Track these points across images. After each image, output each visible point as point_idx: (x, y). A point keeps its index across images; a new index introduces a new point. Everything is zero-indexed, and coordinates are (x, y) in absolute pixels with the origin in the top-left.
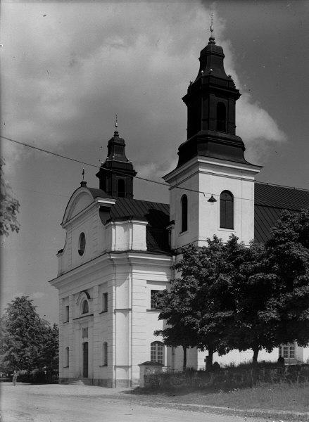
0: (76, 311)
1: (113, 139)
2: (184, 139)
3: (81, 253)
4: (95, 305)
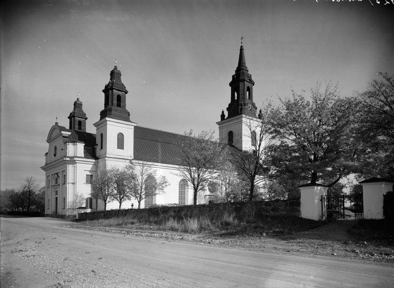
0: (54, 183)
1: (76, 101)
2: (103, 108)
3: (55, 155)
4: (60, 181)
